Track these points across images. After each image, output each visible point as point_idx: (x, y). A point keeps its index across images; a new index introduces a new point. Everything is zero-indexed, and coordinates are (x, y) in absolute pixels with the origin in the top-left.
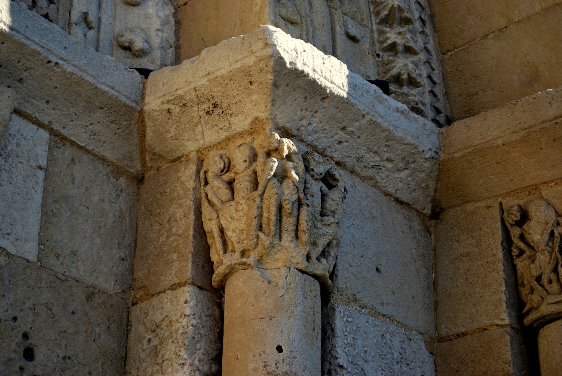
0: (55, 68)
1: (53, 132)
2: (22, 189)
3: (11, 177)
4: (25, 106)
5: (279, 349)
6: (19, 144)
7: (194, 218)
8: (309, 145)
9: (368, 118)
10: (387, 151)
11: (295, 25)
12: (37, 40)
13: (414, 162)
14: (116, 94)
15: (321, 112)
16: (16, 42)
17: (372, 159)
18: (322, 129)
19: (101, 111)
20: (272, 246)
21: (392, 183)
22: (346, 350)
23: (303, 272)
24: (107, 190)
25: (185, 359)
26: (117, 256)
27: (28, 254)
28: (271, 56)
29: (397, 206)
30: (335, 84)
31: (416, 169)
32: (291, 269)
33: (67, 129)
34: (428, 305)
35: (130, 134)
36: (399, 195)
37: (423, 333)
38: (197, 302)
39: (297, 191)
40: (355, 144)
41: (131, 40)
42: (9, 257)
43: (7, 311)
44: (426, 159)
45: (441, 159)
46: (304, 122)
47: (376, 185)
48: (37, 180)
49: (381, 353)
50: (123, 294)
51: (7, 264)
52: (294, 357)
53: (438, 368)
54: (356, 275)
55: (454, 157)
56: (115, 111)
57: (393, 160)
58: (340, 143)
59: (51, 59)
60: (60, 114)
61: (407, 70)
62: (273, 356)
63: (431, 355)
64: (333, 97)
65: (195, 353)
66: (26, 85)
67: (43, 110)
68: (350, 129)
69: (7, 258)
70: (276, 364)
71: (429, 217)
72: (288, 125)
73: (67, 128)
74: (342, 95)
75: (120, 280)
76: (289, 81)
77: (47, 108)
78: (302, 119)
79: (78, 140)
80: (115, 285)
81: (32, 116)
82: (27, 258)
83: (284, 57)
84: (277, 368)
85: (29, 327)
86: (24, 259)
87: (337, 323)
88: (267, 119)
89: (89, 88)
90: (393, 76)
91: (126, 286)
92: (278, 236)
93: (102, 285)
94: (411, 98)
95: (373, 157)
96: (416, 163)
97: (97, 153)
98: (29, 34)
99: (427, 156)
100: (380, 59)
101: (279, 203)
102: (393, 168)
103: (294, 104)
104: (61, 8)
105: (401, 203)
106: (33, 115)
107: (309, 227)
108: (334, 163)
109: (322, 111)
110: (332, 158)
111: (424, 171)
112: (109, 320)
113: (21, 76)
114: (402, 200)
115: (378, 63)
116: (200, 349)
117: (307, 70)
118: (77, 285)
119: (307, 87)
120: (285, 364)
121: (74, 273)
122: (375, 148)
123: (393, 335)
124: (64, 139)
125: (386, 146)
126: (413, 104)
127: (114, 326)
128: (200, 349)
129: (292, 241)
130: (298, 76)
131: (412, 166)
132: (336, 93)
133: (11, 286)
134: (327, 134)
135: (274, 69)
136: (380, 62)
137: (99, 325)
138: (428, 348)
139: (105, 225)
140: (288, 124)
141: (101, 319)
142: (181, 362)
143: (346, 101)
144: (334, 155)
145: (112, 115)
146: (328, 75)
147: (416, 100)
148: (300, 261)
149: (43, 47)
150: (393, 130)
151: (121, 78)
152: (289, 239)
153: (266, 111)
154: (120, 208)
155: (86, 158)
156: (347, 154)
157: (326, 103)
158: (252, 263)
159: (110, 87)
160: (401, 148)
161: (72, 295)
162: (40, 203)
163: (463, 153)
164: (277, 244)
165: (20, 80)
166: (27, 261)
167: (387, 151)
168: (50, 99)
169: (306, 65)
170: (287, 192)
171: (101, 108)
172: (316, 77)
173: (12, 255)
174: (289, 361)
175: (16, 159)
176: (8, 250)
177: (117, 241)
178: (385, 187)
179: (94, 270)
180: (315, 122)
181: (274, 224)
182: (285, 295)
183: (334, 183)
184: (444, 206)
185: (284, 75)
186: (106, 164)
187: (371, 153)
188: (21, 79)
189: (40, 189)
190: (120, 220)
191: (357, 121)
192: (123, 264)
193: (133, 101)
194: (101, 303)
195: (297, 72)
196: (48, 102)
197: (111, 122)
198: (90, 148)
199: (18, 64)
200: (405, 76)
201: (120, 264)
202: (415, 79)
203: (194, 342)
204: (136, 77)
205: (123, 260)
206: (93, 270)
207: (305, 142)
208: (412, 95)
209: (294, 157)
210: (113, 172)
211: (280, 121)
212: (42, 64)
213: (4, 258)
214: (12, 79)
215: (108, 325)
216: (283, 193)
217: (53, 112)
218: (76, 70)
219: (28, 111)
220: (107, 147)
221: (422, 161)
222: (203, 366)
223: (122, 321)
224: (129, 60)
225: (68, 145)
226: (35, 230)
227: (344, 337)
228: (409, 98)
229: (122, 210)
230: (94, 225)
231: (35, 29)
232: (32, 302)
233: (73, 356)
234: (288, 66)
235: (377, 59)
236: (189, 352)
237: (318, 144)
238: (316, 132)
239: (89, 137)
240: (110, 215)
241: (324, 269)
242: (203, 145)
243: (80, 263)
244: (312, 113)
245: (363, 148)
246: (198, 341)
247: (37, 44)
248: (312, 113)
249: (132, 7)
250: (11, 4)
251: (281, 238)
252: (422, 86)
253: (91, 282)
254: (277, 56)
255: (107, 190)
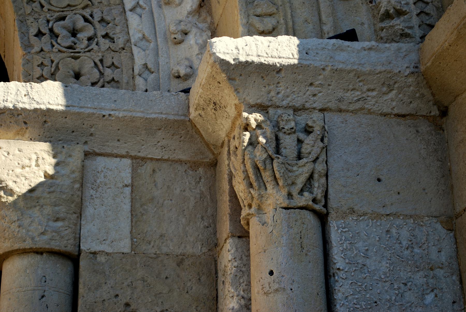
0: (110, 118)
1: (133, 158)
2: (113, 206)
3: (102, 200)
4: (103, 149)
5: (271, 273)
6: (106, 176)
7: (229, 187)
8: (285, 108)
9: (329, 68)
10: (364, 85)
11: (274, 16)
12: (89, 105)
13: (395, 83)
14: (164, 116)
15: (282, 82)
16: (74, 114)
17: (353, 95)
18: (291, 92)
19: (160, 131)
20: (261, 196)
21: (385, 105)
22: (342, 255)
23: (286, 208)
24: (187, 182)
25: (233, 293)
26: (202, 226)
27: (122, 249)
28: (215, 62)
29: (398, 120)
30: (284, 58)
31: (401, 87)
32: (277, 209)
33: (142, 152)
34: (444, 191)
35: (192, 137)
36: (396, 111)
37: (438, 215)
38: (237, 248)
39: (265, 151)
40: (329, 91)
41: (177, 70)
42: (108, 255)
43: (109, 293)
44: (406, 76)
45: (422, 71)
46: (273, 94)
47: (370, 112)
48: (125, 196)
49: (385, 247)
50: (210, 252)
51: (106, 262)
52: (283, 276)
53: (458, 241)
54: (351, 192)
55: (427, 66)
56: (171, 127)
57: (375, 89)
58: (314, 95)
59: (104, 114)
60: (131, 144)
61: (392, 5)
62: (266, 279)
63: (449, 232)
64: (285, 67)
65: (240, 286)
66: (97, 136)
67: (118, 147)
68: (317, 83)
69: (106, 257)
70: (269, 285)
71: (439, 116)
72: (259, 101)
73: (142, 151)
74: (292, 63)
75: (206, 243)
76: (240, 73)
77: (121, 144)
78: (269, 92)
79: (155, 156)
80: (201, 248)
81: (112, 153)
82: (123, 252)
83: (224, 58)
84: (270, 288)
85: (129, 298)
86: (120, 253)
87: (332, 237)
88: (240, 103)
89: (142, 121)
90: (383, 14)
91: (211, 245)
92: (263, 187)
93: (189, 250)
94: (396, 28)
95: (353, 94)
96: (399, 83)
97: (173, 159)
98: (82, 105)
99: (406, 74)
100: (374, 4)
101: (254, 164)
102: (377, 94)
103: (255, 85)
104: (124, 69)
105: (404, 116)
106: (113, 153)
107: (281, 174)
108: (317, 111)
109: (283, 80)
110: (314, 109)
111: (410, 85)
112: (198, 274)
113: (91, 132)
114: (403, 113)
115: (373, 8)
116: (243, 282)
117: (249, 59)
118: (168, 257)
119: (258, 70)
120: (275, 283)
121: (165, 250)
122: (351, 87)
123: (399, 227)
124: (143, 159)
125: (360, 81)
126: (400, 32)
127: (203, 278)
128: (243, 282)
129: (273, 188)
130: (245, 66)
131: (396, 86)
132: (286, 64)
133: (111, 275)
134: (298, 94)
135: (222, 69)
136: (374, 6)
137: (190, 280)
138: (445, 227)
139: (188, 208)
140: (258, 100)
141: (191, 276)
142: (231, 295)
143: (299, 65)
144: (314, 106)
145: (170, 130)
146: (275, 54)
147: (401, 27)
148: (282, 201)
149: (96, 109)
150: (358, 68)
151: (167, 103)
152: (271, 187)
153: (236, 99)
154: (200, 190)
155: (165, 165)
156: (326, 101)
157: (283, 74)
158: (253, 213)
159: (158, 113)
160: (375, 77)
161: (165, 266)
162: (129, 210)
163: (431, 61)
164: (264, 194)
165: (91, 135)
166: (123, 253)
167: (364, 85)
168: (119, 138)
169: (249, 55)
170: (258, 154)
171: (160, 129)
172: (262, 60)
173: (110, 253)
174: (278, 280)
175: (105, 186)
176: (106, 251)
177: (200, 215)
178: (379, 110)
179: (182, 243)
180: (282, 90)
181: (254, 181)
182: (273, 231)
183: (311, 130)
184: (446, 104)
185: (233, 69)
186: (184, 163)
187: (349, 92)
188: (92, 134)
189: (128, 201)
190: (202, 199)
191: (320, 75)
192: (208, 230)
193: (181, 115)
194: (190, 265)
195: (242, 64)
196: (118, 140)
197: (173, 135)
198: (166, 157)
199: (84, 126)
200: (392, 11)
201: (204, 231)
202: (401, 9)
203: (238, 279)
204: (181, 97)
205: (208, 227)
206: (180, 243)
207: (281, 106)
208: (397, 25)
209: (263, 125)
210: (191, 167)
211: (251, 101)
212: (100, 120)
213: (104, 258)
214: (85, 136)
215: (198, 278)
216: (255, 156)
217: (126, 145)
218: (125, 114)
219: (107, 152)
220: (179, 152)
221: (403, 79)
222: (247, 294)
223: (211, 272)
224: (181, 84)
225: (148, 162)
226: (127, 229)
227: (340, 245)
228: (395, 28)
229: (203, 192)
230: (178, 211)
231: (87, 99)
232: (129, 281)
233: (170, 308)
234: (232, 62)
235: (371, 5)
236: (235, 287)
237: (294, 104)
238: (288, 96)
239: (162, 151)
240: (192, 199)
241: (306, 200)
242: (226, 131)
243: (169, 241)
244: (275, 85)
245: (339, 91)
246: (240, 277)
247: (90, 108)
248: (275, 85)
249: (180, 44)
250: (64, 90)
251: (266, 188)
252: (409, 13)
253: (180, 251)
254: (219, 60)
255: (187, 182)
